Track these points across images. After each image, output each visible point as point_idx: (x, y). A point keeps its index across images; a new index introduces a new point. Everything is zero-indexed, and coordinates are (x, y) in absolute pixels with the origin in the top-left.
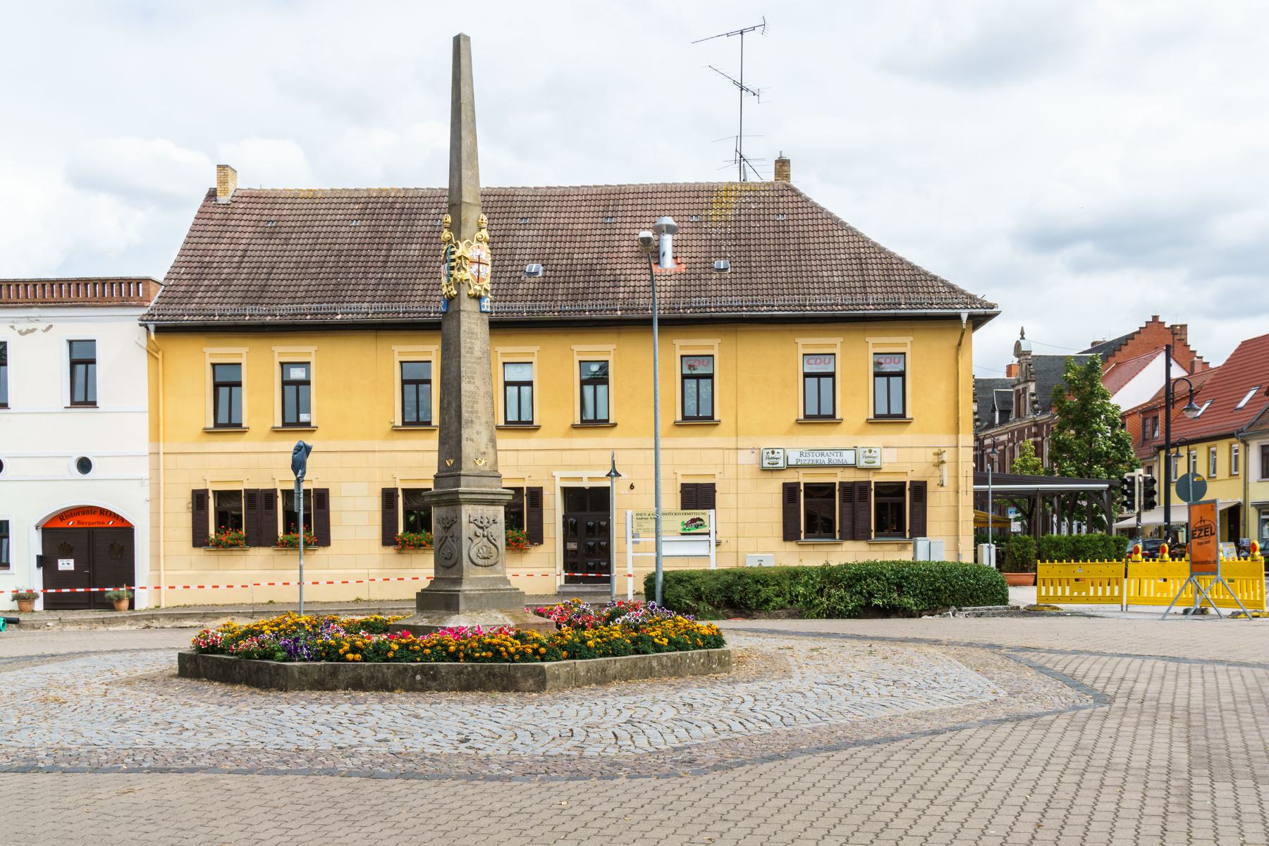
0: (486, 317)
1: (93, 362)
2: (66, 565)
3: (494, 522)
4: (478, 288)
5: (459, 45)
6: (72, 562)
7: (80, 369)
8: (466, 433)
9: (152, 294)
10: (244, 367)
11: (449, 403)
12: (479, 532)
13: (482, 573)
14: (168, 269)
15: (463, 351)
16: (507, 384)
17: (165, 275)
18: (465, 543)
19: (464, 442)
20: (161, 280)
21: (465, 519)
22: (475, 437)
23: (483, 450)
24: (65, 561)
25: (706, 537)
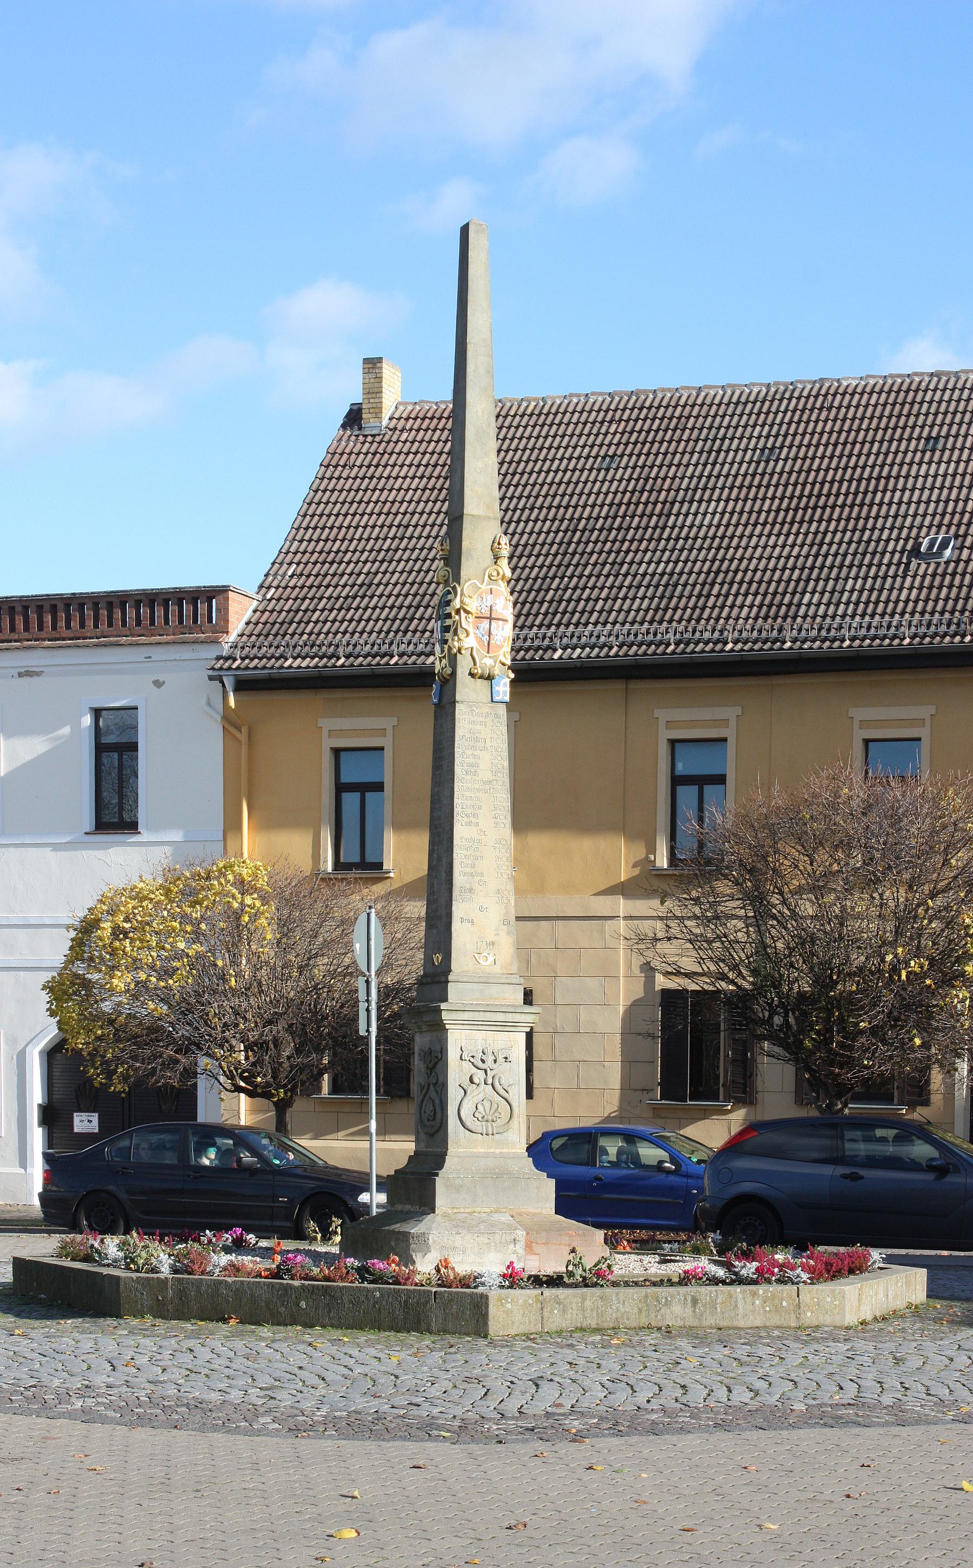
4: (488, 662)
5: (465, 230)
6: (95, 1118)
11: (439, 859)
15: (458, 770)
19: (456, 926)
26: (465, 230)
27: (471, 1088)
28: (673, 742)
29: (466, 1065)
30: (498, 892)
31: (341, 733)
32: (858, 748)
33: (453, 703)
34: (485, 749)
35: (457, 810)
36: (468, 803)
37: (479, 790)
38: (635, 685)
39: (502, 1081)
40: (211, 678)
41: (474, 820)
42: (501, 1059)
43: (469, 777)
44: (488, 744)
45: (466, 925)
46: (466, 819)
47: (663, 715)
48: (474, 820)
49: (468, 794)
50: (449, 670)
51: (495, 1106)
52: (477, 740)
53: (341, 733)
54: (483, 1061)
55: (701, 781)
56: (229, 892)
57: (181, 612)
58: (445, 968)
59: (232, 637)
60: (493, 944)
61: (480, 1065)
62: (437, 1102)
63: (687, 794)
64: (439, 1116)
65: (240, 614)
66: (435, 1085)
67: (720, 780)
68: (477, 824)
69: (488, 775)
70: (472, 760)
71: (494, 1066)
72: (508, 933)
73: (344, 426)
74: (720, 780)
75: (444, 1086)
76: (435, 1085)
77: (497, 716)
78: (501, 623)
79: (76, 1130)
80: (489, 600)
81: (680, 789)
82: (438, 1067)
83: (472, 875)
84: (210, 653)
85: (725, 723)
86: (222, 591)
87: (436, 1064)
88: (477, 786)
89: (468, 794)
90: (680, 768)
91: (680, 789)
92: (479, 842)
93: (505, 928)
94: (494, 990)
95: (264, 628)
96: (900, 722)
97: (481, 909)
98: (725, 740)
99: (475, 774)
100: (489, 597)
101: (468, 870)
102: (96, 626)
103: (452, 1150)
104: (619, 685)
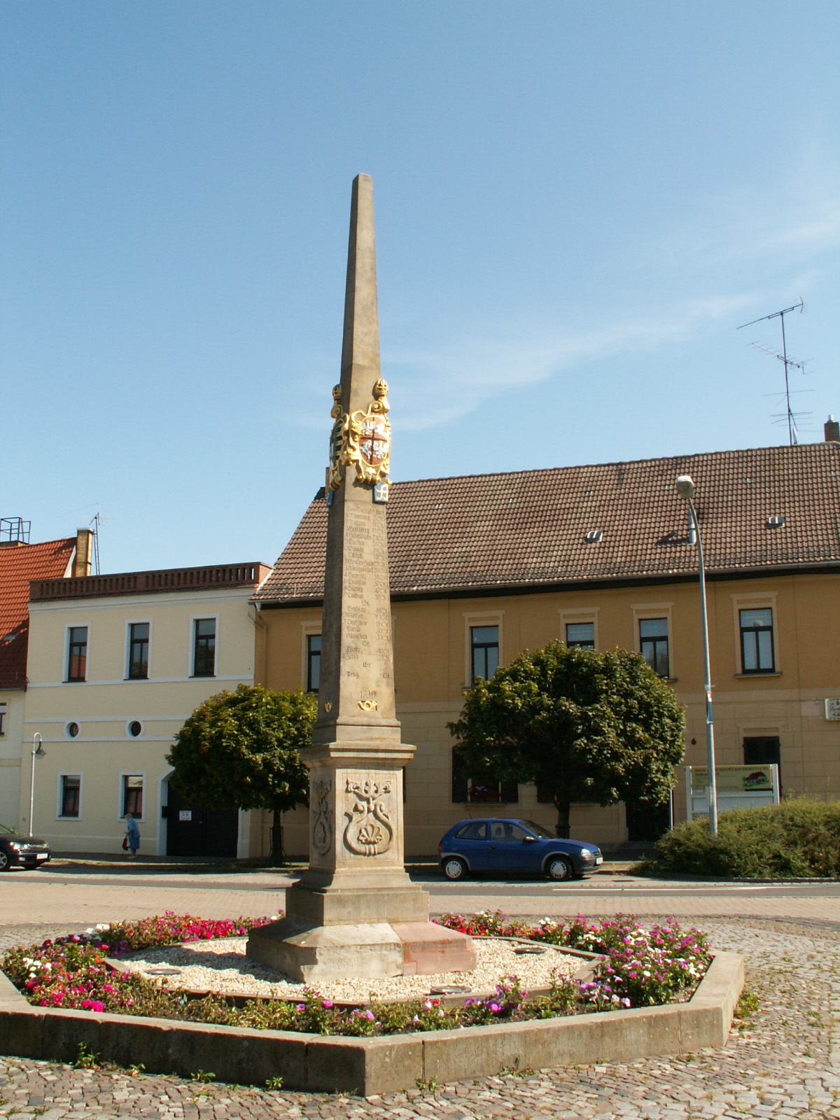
0: (382, 508)
1: (146, 641)
2: (185, 816)
3: (387, 791)
4: (371, 470)
5: (356, 183)
6: (190, 813)
7: (137, 646)
8: (346, 665)
9: (261, 577)
10: (217, 622)
11: (331, 626)
12: (363, 805)
13: (365, 865)
14: (279, 555)
15: (346, 553)
16: (743, 630)
17: (275, 560)
18: (340, 822)
19: (344, 679)
20: (271, 565)
21: (340, 786)
22: (362, 671)
23: (373, 687)
24: (185, 812)
25: (769, 793)
26: (356, 183)
27: (356, 816)
28: (472, 628)
29: (351, 795)
30: (380, 650)
31: (312, 628)
32: (563, 627)
33: (343, 502)
34: (368, 537)
35: (345, 584)
36: (354, 579)
37: (363, 570)
38: (453, 601)
39: (383, 808)
40: (250, 604)
41: (359, 593)
42: (381, 790)
43: (355, 559)
44: (371, 534)
45: (352, 678)
46: (352, 592)
47: (467, 615)
48: (359, 593)
49: (354, 572)
50: (340, 479)
51: (376, 830)
52: (362, 530)
53: (312, 628)
54: (366, 792)
55: (486, 646)
56: (275, 714)
57: (234, 576)
58: (335, 713)
59: (261, 585)
60: (375, 693)
61: (364, 794)
62: (327, 826)
63: (480, 653)
64: (328, 839)
65: (265, 577)
66: (325, 812)
67: (496, 645)
68: (361, 597)
69: (371, 558)
70: (358, 546)
71: (376, 795)
72: (388, 685)
73: (316, 498)
74: (496, 645)
75: (333, 812)
76: (325, 812)
77: (378, 512)
78: (381, 442)
79: (181, 819)
80: (371, 426)
81: (476, 650)
82: (328, 799)
83: (357, 637)
84: (251, 592)
85: (497, 618)
86: (256, 566)
87: (326, 794)
88: (361, 566)
89: (354, 572)
90: (476, 640)
91: (476, 650)
92: (364, 610)
93: (385, 680)
94: (376, 732)
95: (274, 585)
96: (582, 615)
97: (365, 664)
98: (497, 626)
99: (361, 557)
100: (372, 423)
101: (354, 633)
102: (198, 582)
103: (339, 870)
104: (445, 602)
